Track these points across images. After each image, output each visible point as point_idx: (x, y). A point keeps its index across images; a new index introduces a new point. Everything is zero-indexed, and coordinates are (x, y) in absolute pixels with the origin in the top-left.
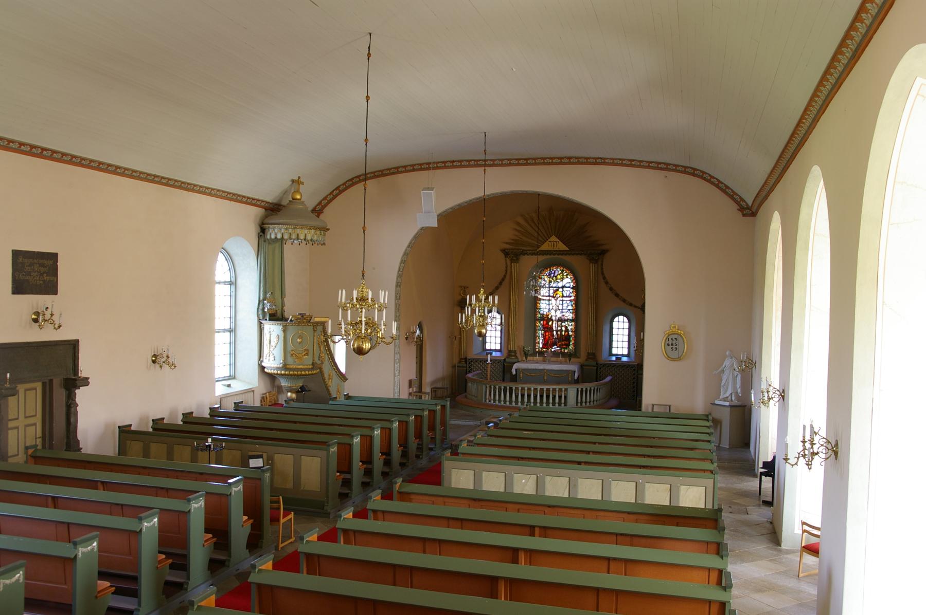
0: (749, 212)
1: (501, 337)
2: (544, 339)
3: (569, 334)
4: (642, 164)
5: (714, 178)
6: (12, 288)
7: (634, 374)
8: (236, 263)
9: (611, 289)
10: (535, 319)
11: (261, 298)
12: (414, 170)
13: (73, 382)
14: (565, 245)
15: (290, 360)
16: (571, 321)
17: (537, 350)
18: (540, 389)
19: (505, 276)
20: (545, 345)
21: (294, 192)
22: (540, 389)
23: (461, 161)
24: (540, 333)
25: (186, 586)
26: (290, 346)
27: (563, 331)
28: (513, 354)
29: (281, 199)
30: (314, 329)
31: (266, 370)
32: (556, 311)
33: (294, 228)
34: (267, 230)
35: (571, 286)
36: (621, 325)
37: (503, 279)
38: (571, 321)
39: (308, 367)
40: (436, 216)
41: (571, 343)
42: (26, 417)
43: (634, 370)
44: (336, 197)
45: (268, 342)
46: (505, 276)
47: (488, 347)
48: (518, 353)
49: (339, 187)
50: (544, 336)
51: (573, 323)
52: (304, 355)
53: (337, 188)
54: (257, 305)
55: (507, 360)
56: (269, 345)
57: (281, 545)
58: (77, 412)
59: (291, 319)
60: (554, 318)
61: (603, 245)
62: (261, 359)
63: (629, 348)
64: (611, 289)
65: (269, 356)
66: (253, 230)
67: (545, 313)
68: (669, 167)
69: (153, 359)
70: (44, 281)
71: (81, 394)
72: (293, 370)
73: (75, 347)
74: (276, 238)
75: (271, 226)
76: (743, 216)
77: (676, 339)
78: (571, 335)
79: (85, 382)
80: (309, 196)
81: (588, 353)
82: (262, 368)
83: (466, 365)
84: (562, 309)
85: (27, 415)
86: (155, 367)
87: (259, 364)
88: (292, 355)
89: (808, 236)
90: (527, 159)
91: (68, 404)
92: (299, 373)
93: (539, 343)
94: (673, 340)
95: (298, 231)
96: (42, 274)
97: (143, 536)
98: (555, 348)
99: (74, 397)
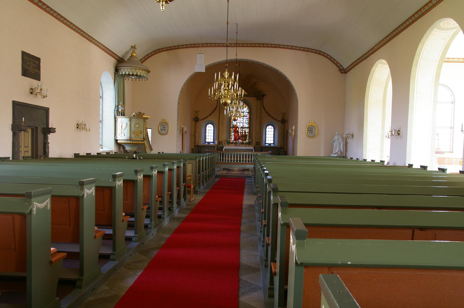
0: (343, 71)
1: (214, 136)
2: (235, 136)
3: (246, 134)
4: (297, 48)
5: (329, 55)
6: (22, 72)
7: (278, 151)
8: (103, 86)
9: (267, 113)
10: (230, 127)
11: (116, 105)
12: (187, 47)
13: (48, 130)
14: (246, 92)
15: (133, 136)
16: (247, 128)
17: (231, 142)
18: (245, 154)
19: (217, 106)
20: (235, 139)
21: (132, 52)
22: (245, 154)
23: (211, 44)
24: (233, 134)
25: (172, 209)
26: (133, 129)
27: (243, 133)
28: (221, 143)
29: (124, 56)
30: (144, 121)
31: (118, 142)
32: (240, 123)
33: (136, 69)
34: (120, 70)
35: (247, 112)
36: (270, 130)
37: (216, 108)
38: (247, 128)
39: (141, 139)
40: (205, 67)
41: (247, 138)
42: (25, 147)
43: (278, 149)
44: (147, 59)
45: (121, 127)
46: (217, 106)
47: (207, 141)
48: (223, 142)
49: (148, 54)
50: (235, 135)
51: (248, 129)
52: (140, 133)
53: (147, 55)
54: (114, 108)
55: (218, 146)
56: (121, 128)
57: (192, 200)
58: (49, 147)
59: (134, 115)
60: (239, 127)
61: (263, 92)
62: (116, 136)
63: (274, 140)
64: (267, 113)
65: (121, 134)
66: (113, 70)
67: (235, 124)
68: (309, 50)
69: (77, 126)
70: (35, 72)
71: (51, 137)
72: (134, 141)
73: (47, 111)
74: (125, 74)
75: (123, 68)
76: (341, 73)
77: (312, 128)
78: (247, 135)
79: (52, 130)
80: (139, 53)
81: (257, 142)
82: (116, 141)
83: (198, 149)
84: (243, 123)
85: (25, 146)
86: (78, 131)
87: (115, 139)
88: (134, 133)
89: (419, 59)
90: (243, 44)
91: (45, 142)
92: (137, 142)
93: (232, 139)
94: (310, 129)
95: (137, 71)
96: (34, 68)
97: (166, 175)
98: (240, 141)
99: (47, 139)
